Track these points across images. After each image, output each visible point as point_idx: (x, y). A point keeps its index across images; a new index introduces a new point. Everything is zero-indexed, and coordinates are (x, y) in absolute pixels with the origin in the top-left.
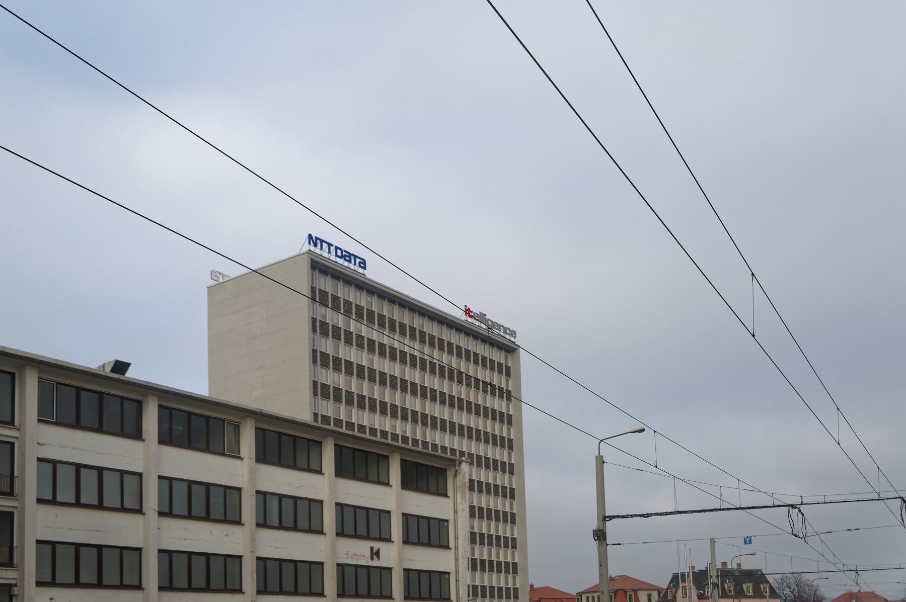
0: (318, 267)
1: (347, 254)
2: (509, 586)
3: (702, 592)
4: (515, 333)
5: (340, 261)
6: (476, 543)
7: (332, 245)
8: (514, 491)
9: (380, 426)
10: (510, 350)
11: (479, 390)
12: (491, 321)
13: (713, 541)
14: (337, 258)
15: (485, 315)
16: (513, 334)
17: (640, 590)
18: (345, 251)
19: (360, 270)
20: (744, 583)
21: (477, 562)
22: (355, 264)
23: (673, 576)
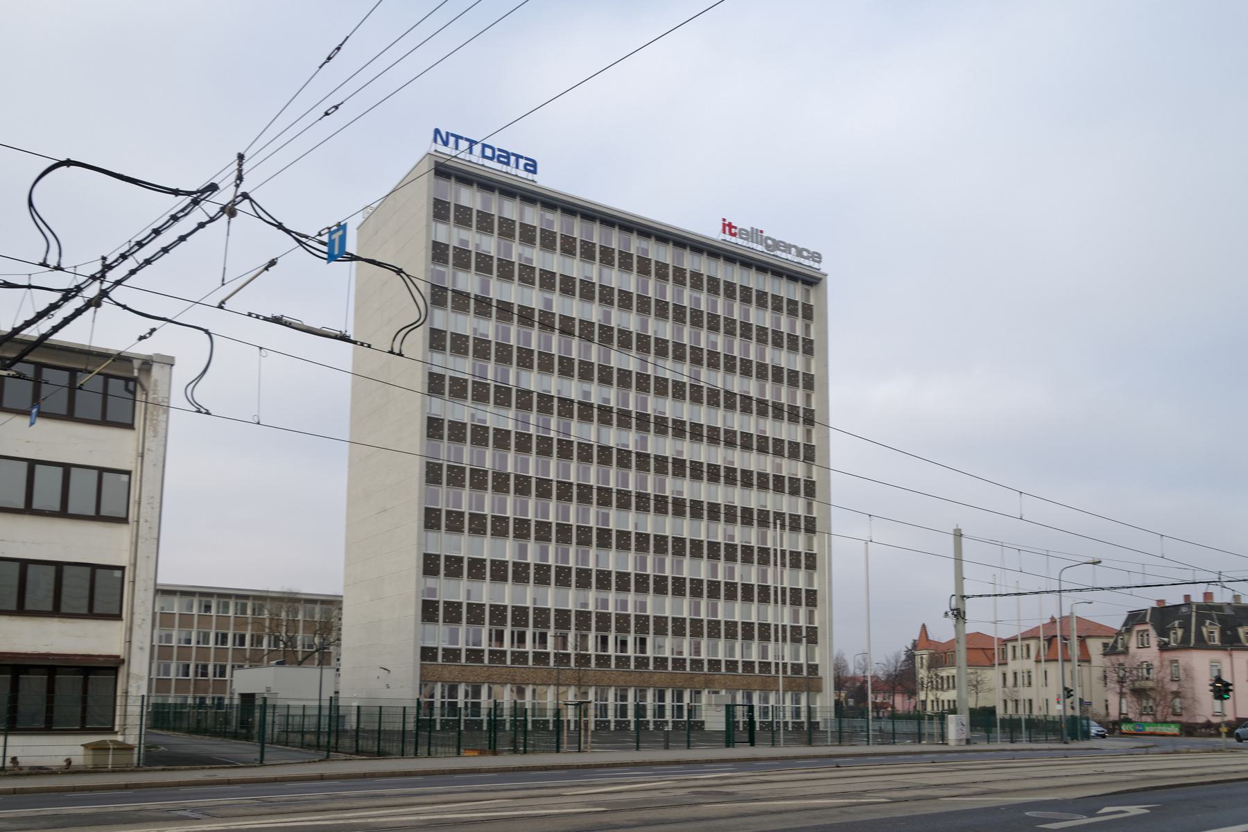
0: (443, 171)
1: (530, 163)
2: (800, 624)
3: (1166, 639)
4: (819, 256)
5: (494, 164)
6: (736, 561)
7: (476, 143)
8: (814, 486)
9: (741, 426)
10: (811, 281)
11: (751, 339)
12: (773, 240)
13: (958, 535)
14: (485, 160)
15: (762, 232)
16: (817, 257)
17: (1090, 637)
18: (500, 150)
19: (530, 176)
20: (1241, 625)
21: (736, 588)
22: (517, 167)
23: (1129, 615)
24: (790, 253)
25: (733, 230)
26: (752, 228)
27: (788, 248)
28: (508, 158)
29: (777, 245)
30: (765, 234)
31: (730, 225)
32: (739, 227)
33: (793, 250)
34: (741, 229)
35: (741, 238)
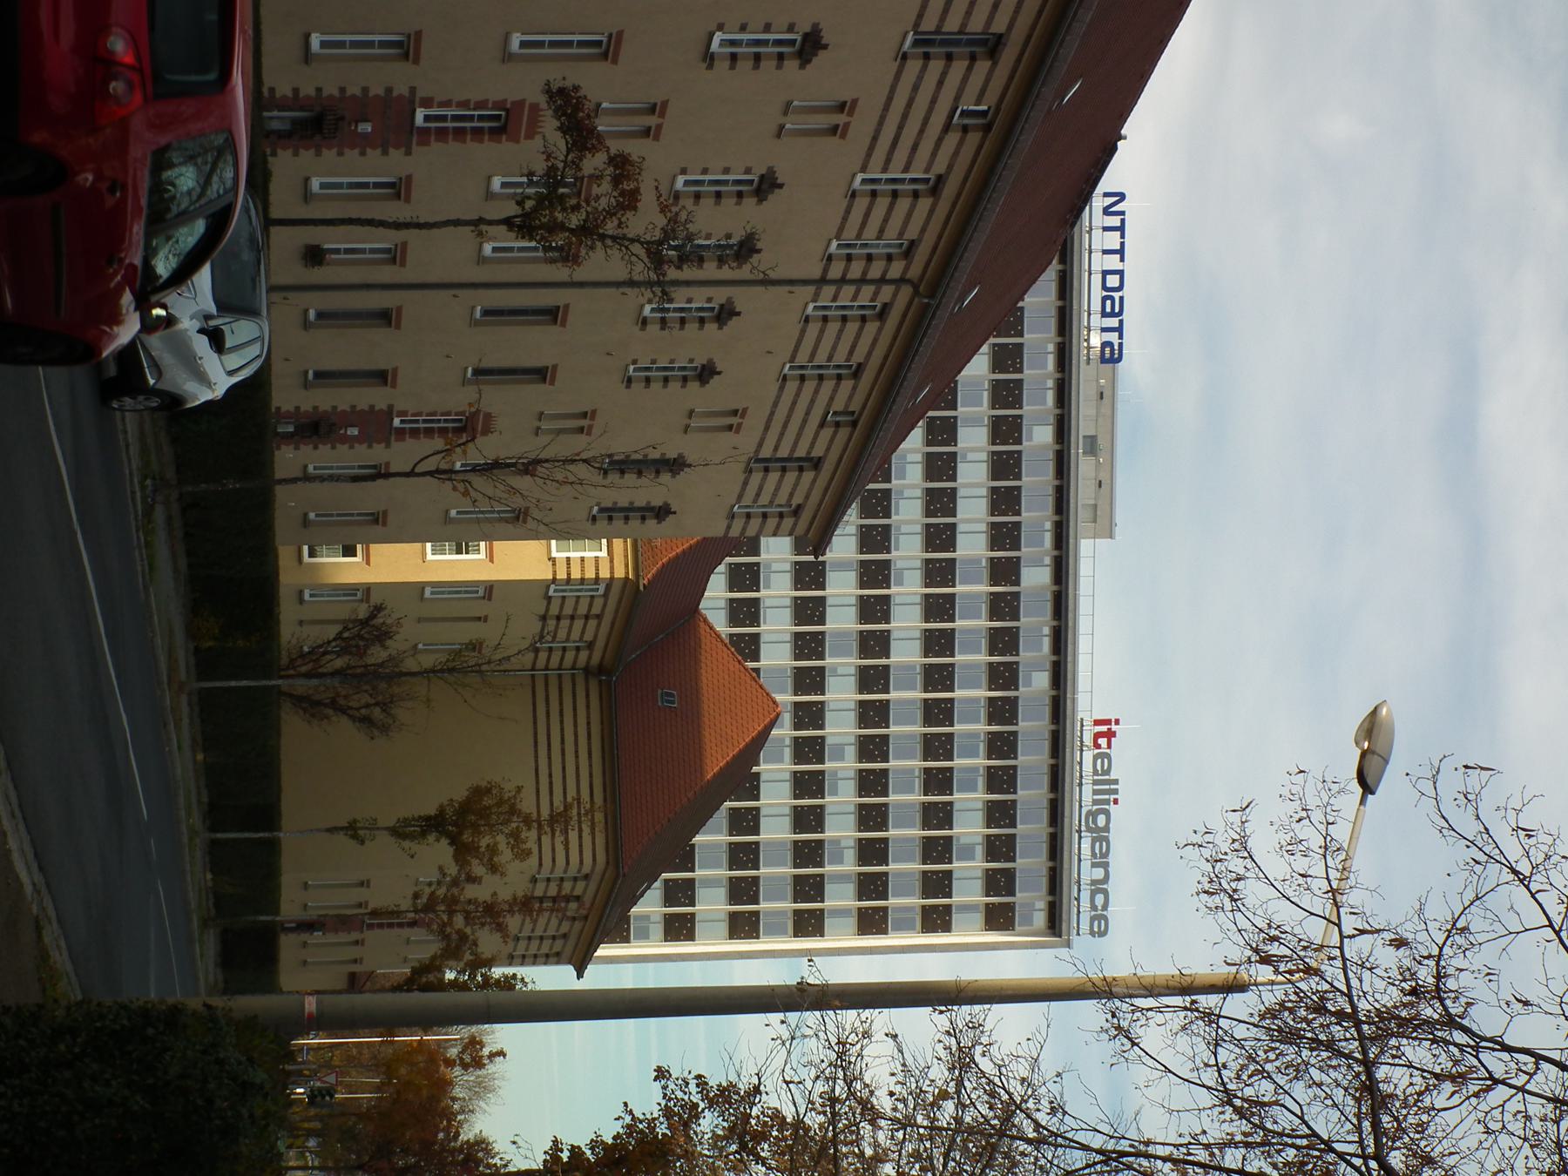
7: (1122, 260)
12: (1107, 829)
15: (1116, 801)
18: (1121, 299)
24: (1094, 865)
25: (1103, 741)
26: (1116, 782)
27: (1101, 860)
28: (1113, 314)
29: (1101, 836)
30: (1112, 808)
31: (1110, 735)
32: (1113, 752)
33: (1099, 873)
34: (1108, 756)
35: (1095, 758)
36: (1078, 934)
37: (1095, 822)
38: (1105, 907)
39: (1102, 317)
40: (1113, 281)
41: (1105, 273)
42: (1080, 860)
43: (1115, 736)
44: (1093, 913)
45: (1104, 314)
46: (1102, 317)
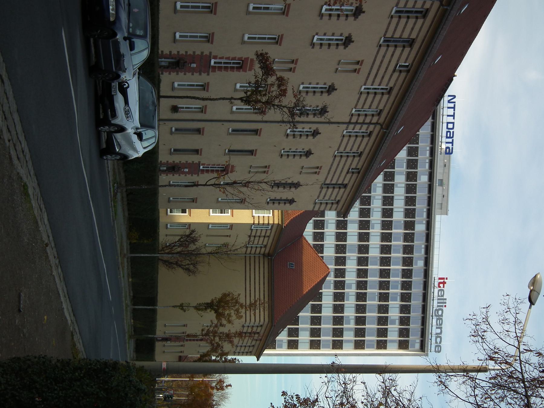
7: (454, 119)
12: (442, 315)
15: (445, 306)
18: (453, 132)
19: (433, 349)
25: (441, 285)
26: (446, 299)
28: (450, 137)
29: (440, 318)
30: (444, 308)
31: (444, 283)
32: (445, 289)
33: (438, 331)
34: (443, 290)
36: (431, 352)
37: (438, 313)
38: (440, 342)
39: (446, 138)
40: (450, 126)
41: (448, 123)
42: (432, 326)
43: (446, 284)
44: (436, 344)
45: (447, 137)
46: (446, 138)
